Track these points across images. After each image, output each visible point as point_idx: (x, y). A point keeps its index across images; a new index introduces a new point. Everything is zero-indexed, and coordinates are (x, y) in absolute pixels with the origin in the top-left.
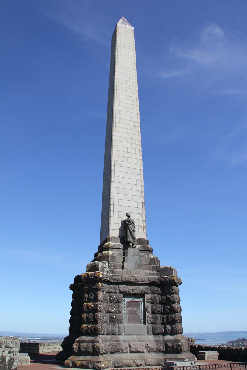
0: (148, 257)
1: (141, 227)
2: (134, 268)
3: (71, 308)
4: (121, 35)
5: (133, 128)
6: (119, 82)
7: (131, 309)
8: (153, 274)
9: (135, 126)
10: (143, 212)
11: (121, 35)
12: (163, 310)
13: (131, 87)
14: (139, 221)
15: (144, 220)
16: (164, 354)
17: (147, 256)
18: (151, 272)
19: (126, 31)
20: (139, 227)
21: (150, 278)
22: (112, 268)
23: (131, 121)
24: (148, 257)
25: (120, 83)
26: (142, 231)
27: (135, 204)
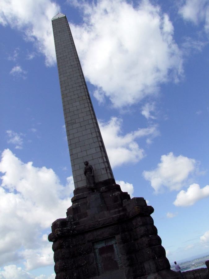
0: (113, 195)
1: (103, 169)
2: (97, 212)
3: (53, 253)
4: (63, 71)
5: (78, 88)
6: (60, 60)
7: (105, 255)
8: (119, 212)
9: (80, 86)
10: (102, 154)
11: (63, 71)
12: (96, 228)
13: (71, 58)
14: (105, 163)
15: (105, 162)
16: (38, 169)
17: (111, 195)
18: (116, 210)
19: (59, 21)
20: (102, 170)
21: (115, 217)
22: (77, 219)
23: (76, 83)
24: (113, 195)
25: (61, 60)
26: (106, 172)
27: (93, 151)
